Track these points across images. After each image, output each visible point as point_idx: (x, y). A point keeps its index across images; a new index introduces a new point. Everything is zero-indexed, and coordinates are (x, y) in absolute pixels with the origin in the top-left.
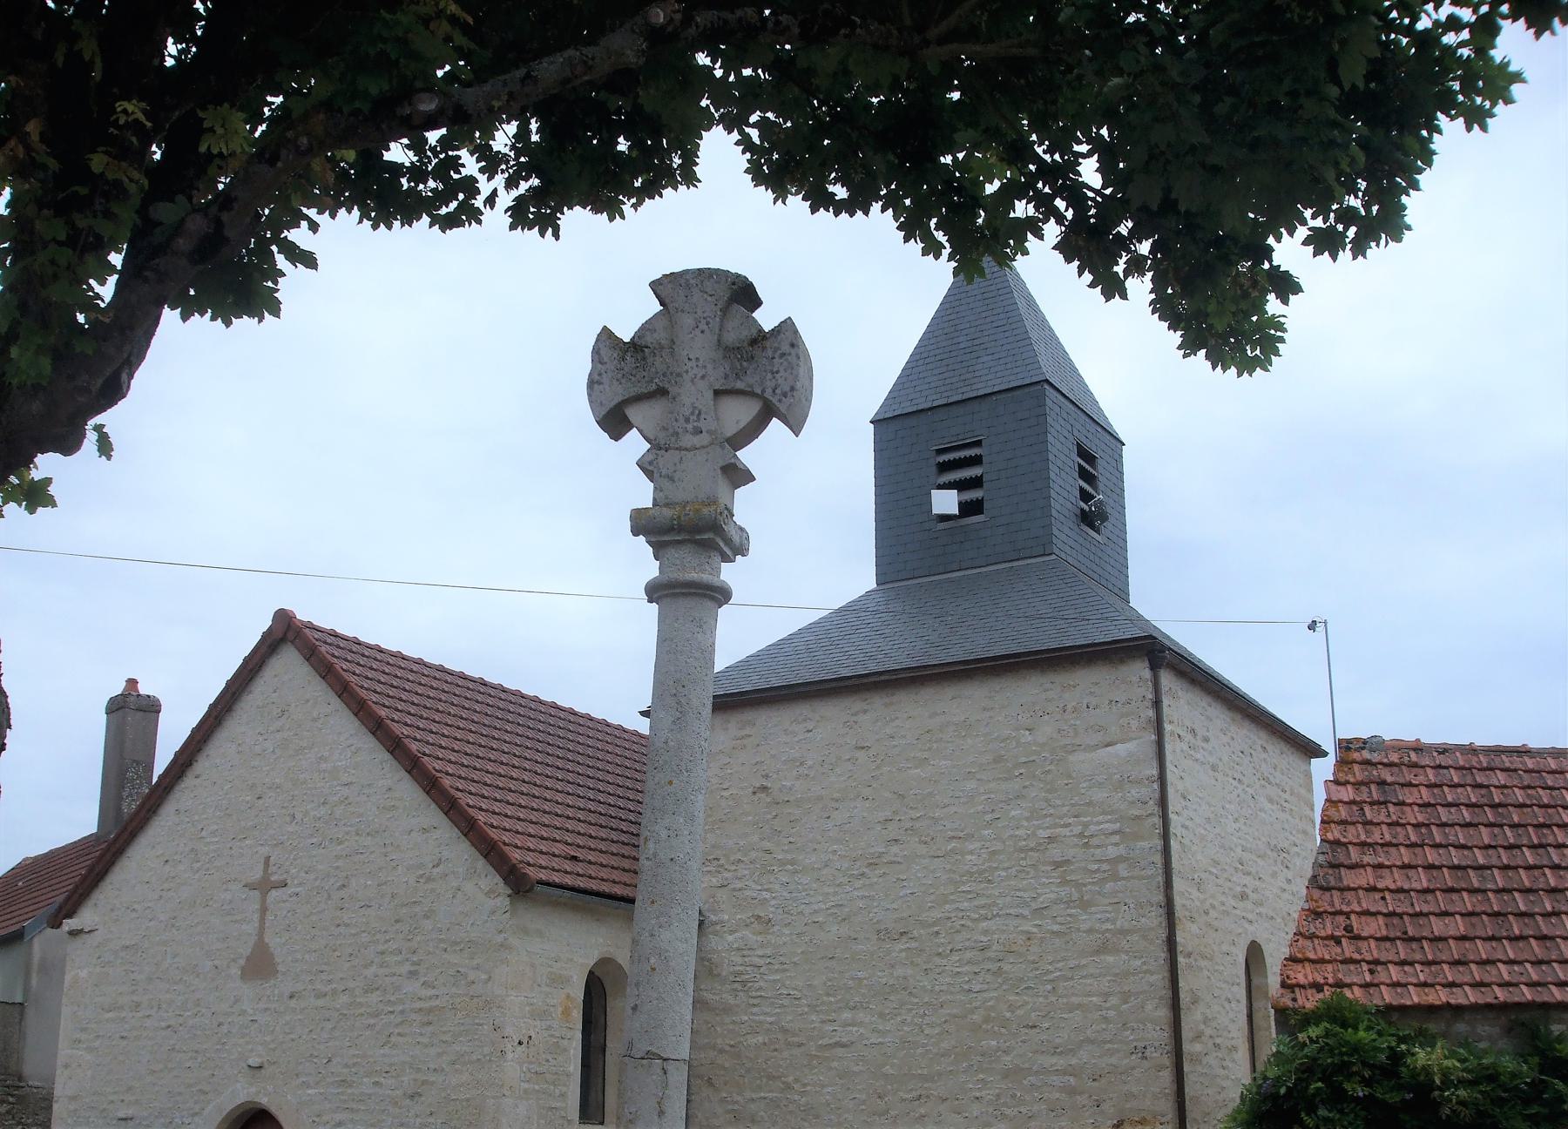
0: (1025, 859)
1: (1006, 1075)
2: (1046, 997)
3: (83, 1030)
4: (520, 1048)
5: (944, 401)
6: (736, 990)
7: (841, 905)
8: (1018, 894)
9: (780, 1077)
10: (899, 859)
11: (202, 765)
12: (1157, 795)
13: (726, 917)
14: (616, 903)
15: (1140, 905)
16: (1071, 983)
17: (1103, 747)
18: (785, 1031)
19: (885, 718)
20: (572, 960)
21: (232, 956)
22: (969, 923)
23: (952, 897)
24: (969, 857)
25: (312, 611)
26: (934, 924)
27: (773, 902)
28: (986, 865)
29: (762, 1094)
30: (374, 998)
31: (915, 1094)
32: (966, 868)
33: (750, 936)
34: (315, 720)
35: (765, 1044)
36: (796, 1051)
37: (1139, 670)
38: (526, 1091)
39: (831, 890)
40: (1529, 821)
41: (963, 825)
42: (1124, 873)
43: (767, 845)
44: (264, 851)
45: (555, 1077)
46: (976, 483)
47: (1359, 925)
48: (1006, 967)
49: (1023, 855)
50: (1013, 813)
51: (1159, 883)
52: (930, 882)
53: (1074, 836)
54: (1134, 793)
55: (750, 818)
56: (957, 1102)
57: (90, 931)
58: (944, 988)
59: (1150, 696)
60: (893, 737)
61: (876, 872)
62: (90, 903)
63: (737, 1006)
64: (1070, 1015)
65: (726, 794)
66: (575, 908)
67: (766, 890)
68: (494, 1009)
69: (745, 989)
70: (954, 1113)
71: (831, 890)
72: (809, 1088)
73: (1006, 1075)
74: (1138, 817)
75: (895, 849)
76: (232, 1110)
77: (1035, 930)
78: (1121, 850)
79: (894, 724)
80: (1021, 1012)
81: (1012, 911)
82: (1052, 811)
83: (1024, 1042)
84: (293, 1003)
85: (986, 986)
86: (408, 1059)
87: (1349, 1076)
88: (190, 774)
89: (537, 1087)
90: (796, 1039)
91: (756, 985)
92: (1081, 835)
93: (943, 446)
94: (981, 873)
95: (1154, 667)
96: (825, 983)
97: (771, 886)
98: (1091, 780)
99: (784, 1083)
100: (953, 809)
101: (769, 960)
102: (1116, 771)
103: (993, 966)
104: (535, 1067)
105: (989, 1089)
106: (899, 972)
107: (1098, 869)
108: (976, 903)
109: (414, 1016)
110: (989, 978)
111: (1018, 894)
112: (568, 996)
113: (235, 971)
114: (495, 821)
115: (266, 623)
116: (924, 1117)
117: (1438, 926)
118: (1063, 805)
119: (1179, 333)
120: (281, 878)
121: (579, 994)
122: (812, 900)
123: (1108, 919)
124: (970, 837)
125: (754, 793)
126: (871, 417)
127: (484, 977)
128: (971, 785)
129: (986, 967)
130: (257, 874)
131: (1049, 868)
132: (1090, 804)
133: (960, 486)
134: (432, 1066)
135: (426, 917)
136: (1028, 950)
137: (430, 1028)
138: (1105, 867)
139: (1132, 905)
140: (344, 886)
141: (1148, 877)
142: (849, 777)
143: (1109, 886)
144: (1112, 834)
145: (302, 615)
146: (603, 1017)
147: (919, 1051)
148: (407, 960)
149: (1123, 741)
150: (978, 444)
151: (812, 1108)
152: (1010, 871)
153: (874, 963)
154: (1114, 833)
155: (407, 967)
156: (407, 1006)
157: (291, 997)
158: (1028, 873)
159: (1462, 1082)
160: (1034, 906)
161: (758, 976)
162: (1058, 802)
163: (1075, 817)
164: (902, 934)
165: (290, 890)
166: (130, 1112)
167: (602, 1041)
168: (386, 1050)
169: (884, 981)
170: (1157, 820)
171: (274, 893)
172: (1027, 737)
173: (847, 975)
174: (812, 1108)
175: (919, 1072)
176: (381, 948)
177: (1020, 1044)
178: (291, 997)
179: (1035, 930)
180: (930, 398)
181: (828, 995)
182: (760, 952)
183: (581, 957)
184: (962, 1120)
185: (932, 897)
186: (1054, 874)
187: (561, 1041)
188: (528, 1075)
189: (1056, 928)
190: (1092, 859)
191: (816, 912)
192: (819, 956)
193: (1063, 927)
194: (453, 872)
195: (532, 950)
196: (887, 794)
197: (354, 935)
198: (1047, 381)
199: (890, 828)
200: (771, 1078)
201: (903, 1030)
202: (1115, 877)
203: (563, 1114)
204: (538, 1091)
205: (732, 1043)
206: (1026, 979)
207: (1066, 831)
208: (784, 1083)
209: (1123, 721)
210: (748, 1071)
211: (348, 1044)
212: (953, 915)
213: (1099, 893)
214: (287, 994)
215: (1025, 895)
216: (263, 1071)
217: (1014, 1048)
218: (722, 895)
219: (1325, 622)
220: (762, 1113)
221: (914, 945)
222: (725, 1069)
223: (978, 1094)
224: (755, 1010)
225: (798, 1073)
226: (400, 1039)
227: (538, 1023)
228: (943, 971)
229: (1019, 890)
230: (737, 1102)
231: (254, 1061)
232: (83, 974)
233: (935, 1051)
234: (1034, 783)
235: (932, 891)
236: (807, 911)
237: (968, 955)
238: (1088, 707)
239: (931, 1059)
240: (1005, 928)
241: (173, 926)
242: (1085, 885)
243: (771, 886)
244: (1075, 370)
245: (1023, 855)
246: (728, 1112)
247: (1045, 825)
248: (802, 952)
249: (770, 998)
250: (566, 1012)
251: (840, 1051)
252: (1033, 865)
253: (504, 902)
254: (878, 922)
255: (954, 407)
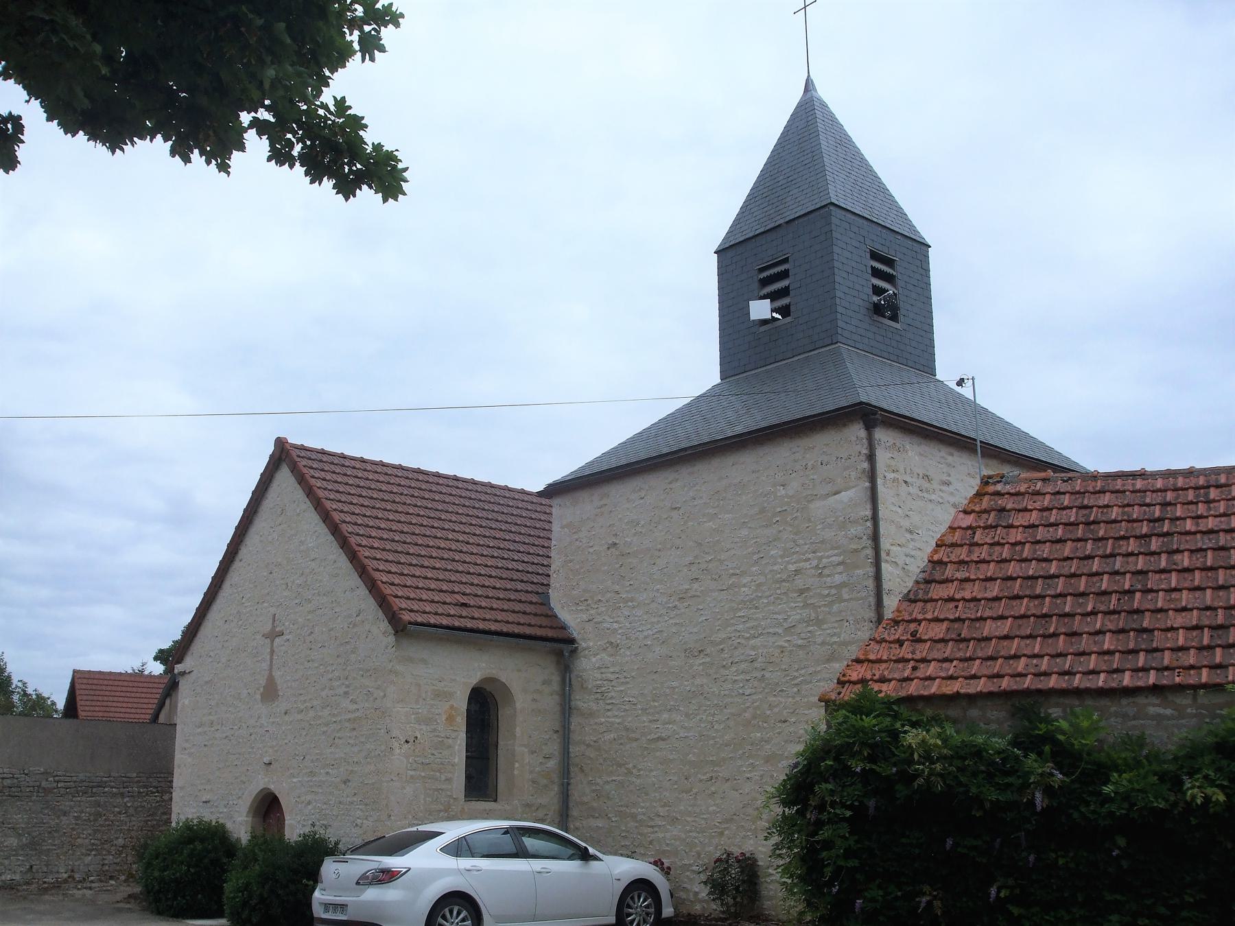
0: (779, 588)
1: (767, 760)
2: (793, 697)
3: (187, 741)
4: (406, 746)
5: (762, 230)
6: (597, 699)
7: (662, 631)
8: (775, 616)
9: (624, 765)
10: (698, 594)
11: (244, 552)
12: (870, 531)
13: (591, 644)
14: (490, 637)
15: (857, 622)
16: (810, 686)
17: (832, 496)
18: (627, 730)
19: (690, 484)
20: (454, 680)
21: (257, 686)
22: (743, 641)
23: (732, 621)
24: (743, 589)
25: (301, 436)
26: (721, 643)
27: (620, 631)
28: (754, 594)
29: (614, 778)
30: (326, 712)
31: (708, 775)
32: (741, 598)
33: (606, 657)
34: (299, 514)
35: (615, 739)
36: (634, 744)
37: (857, 431)
38: (412, 777)
39: (655, 620)
40: (1112, 534)
41: (739, 564)
42: (846, 596)
43: (617, 588)
44: (273, 610)
45: (441, 766)
46: (785, 292)
47: (926, 631)
48: (768, 675)
49: (778, 586)
50: (772, 553)
51: (870, 602)
52: (717, 611)
53: (812, 568)
54: (854, 530)
55: (606, 568)
56: (735, 782)
57: (189, 672)
58: (727, 692)
59: (865, 451)
60: (695, 499)
61: (684, 604)
62: (189, 653)
63: (599, 711)
64: (810, 711)
65: (591, 550)
66: (459, 642)
67: (616, 622)
68: (387, 718)
69: (603, 698)
70: (733, 790)
71: (655, 620)
72: (642, 772)
73: (767, 760)
74: (856, 551)
75: (696, 586)
76: (257, 795)
77: (786, 645)
78: (844, 578)
79: (695, 488)
80: (776, 710)
81: (771, 630)
82: (797, 550)
83: (779, 733)
84: (287, 718)
85: (754, 691)
86: (343, 756)
87: (853, 756)
88: (237, 559)
89: (423, 774)
90: (633, 735)
91: (610, 695)
92: (817, 567)
93: (766, 264)
94: (751, 601)
95: (869, 427)
96: (652, 692)
97: (619, 619)
98: (823, 523)
99: (626, 769)
100: (733, 552)
101: (617, 676)
102: (840, 514)
103: (759, 675)
104: (420, 760)
105: (756, 771)
106: (698, 681)
107: (828, 594)
108: (747, 625)
109: (347, 724)
110: (756, 683)
111: (775, 616)
112: (452, 707)
113: (258, 697)
114: (390, 578)
115: (270, 449)
116: (714, 793)
117: (988, 628)
118: (806, 544)
119: (81, 133)
120: (281, 629)
121: (463, 705)
122: (644, 628)
123: (835, 634)
124: (743, 573)
125: (609, 548)
126: (715, 248)
127: (382, 694)
128: (745, 532)
129: (755, 675)
130: (268, 628)
131: (795, 595)
132: (822, 542)
133: (773, 296)
134: (355, 760)
135: (353, 652)
136: (781, 661)
137: (355, 733)
138: (833, 591)
139: (852, 622)
140: (312, 633)
141: (862, 599)
142: (666, 533)
143: (835, 607)
144: (838, 565)
145: (293, 440)
146: (496, 721)
147: (711, 742)
148: (343, 684)
149: (846, 489)
150: (786, 261)
151: (644, 788)
152: (769, 599)
153: (682, 675)
154: (839, 564)
155: (344, 689)
156: (343, 717)
157: (286, 713)
158: (782, 599)
159: (942, 758)
160: (786, 625)
161: (611, 688)
162: (801, 542)
163: (814, 552)
164: (700, 652)
165: (285, 637)
166: (208, 797)
167: (496, 739)
168: (332, 749)
169: (688, 688)
170: (870, 552)
171: (277, 640)
172: (782, 491)
173: (666, 685)
174: (644, 788)
175: (711, 759)
176: (330, 676)
177: (776, 735)
178: (286, 713)
179: (786, 645)
180: (754, 229)
181: (654, 701)
182: (611, 670)
183: (463, 677)
184: (738, 796)
185: (720, 622)
186: (799, 600)
187: (446, 740)
188: (415, 765)
189: (800, 642)
190: (824, 586)
191: (646, 637)
192: (648, 671)
193: (805, 641)
194: (367, 619)
195: (418, 674)
196: (691, 543)
197: (317, 667)
198: (832, 204)
199: (693, 570)
200: (620, 765)
201: (700, 727)
202: (841, 600)
203: (449, 793)
204: (424, 777)
205: (595, 739)
206: (780, 683)
207: (807, 565)
208: (626, 769)
209: (846, 473)
210: (605, 760)
211: (314, 746)
212: (733, 635)
213: (829, 613)
214: (283, 712)
215: (779, 617)
216: (272, 766)
217: (772, 738)
218: (589, 627)
219: (973, 379)
220: (613, 792)
221: (708, 659)
222: (591, 759)
223: (749, 776)
224: (609, 714)
225: (635, 761)
226: (341, 741)
227: (424, 727)
228: (726, 680)
229: (776, 613)
230: (598, 784)
231: (266, 760)
232: (187, 702)
233: (721, 742)
234: (787, 528)
235: (719, 617)
236: (641, 636)
237: (743, 666)
238: (822, 464)
239: (718, 748)
240: (766, 644)
241: (229, 666)
242: (820, 607)
243: (619, 619)
244: (885, 191)
245: (778, 586)
246: (594, 791)
247: (793, 561)
248: (638, 669)
249: (617, 704)
250: (450, 719)
251: (661, 744)
252: (785, 593)
253: (392, 639)
254: (684, 643)
255: (760, 237)
